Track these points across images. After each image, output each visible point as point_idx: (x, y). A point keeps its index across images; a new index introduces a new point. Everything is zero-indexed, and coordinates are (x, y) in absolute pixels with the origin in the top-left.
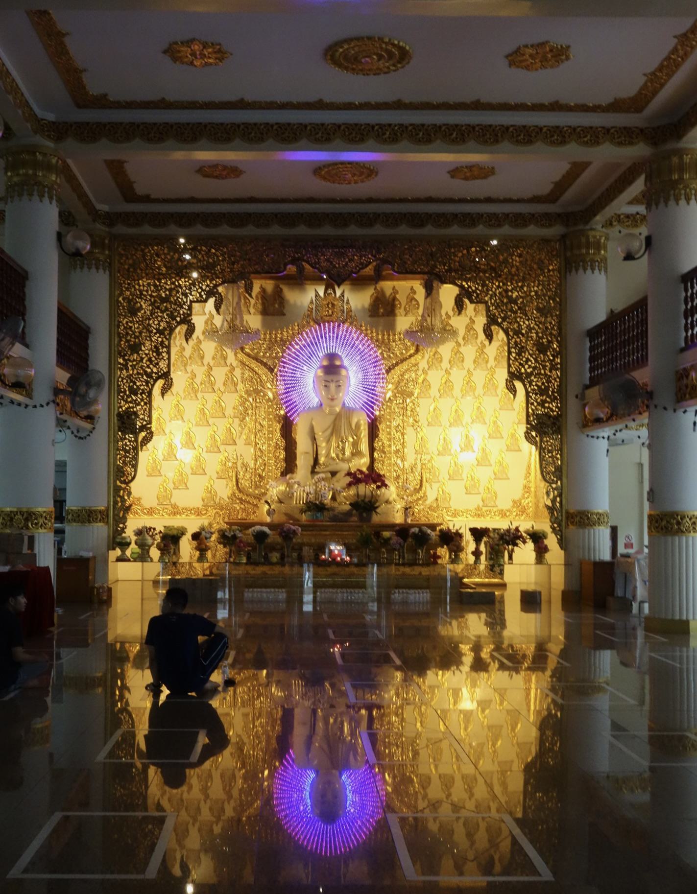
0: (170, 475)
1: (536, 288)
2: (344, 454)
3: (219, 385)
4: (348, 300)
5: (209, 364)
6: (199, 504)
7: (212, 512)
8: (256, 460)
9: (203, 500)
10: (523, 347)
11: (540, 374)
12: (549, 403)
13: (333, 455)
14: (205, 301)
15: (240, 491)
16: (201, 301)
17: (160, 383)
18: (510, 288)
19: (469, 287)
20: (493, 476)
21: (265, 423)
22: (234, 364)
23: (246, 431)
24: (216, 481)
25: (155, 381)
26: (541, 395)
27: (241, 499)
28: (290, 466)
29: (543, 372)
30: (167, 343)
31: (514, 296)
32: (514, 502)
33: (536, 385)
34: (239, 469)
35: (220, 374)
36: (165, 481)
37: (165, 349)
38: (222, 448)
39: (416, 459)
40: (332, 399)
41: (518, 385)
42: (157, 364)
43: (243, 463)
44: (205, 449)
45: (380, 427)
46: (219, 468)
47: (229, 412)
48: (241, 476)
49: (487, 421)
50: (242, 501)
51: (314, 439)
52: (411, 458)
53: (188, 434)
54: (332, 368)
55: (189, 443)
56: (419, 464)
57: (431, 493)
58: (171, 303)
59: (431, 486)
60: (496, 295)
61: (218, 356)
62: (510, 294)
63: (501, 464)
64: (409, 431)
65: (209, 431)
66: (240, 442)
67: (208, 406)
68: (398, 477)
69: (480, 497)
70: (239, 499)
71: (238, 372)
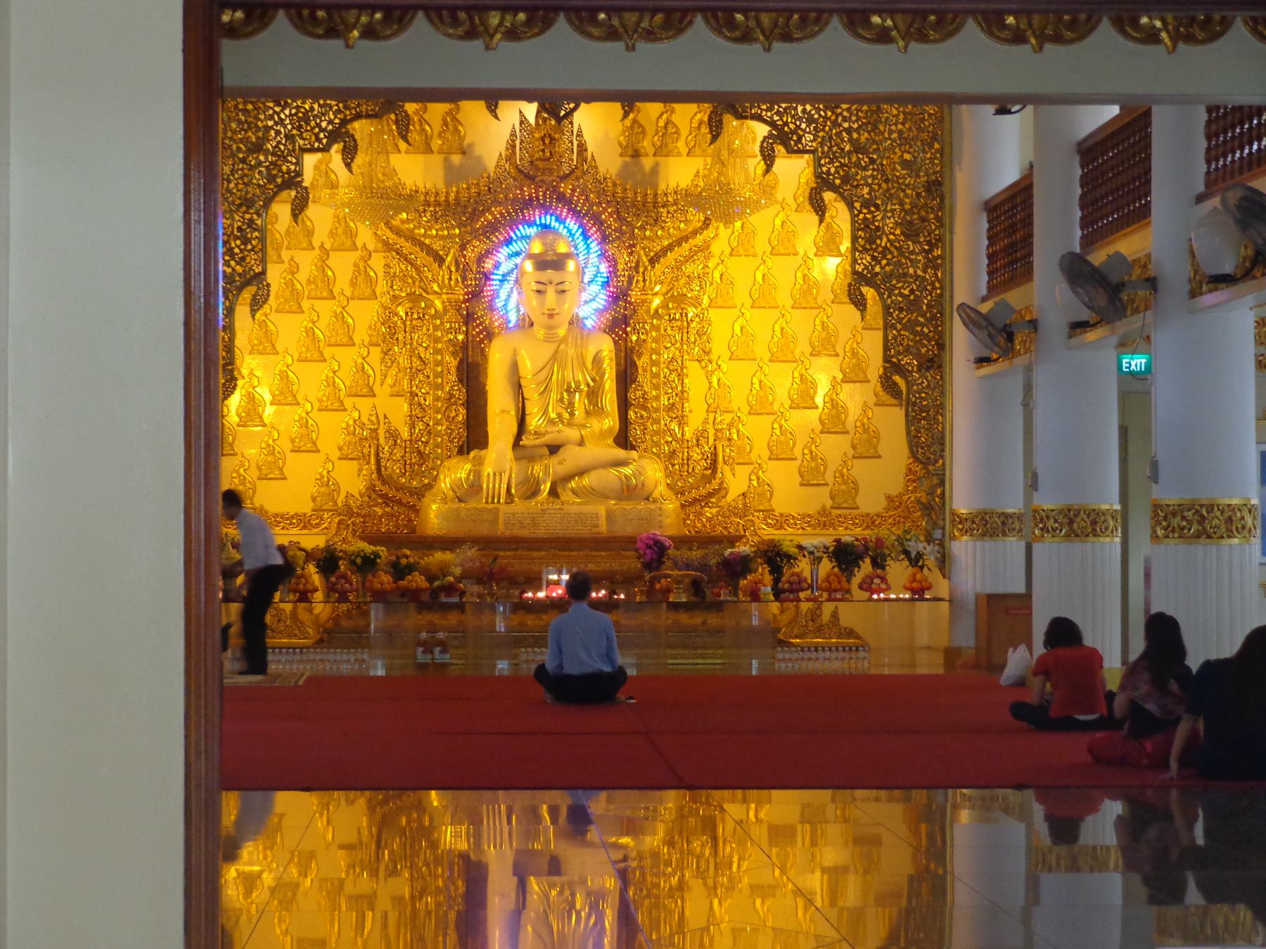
0: (252, 452)
1: (900, 126)
2: (572, 414)
3: (342, 284)
4: (580, 131)
5: (322, 246)
6: (307, 508)
7: (331, 521)
8: (413, 426)
9: (314, 500)
10: (878, 228)
11: (905, 275)
12: (922, 325)
13: (553, 415)
14: (326, 149)
15: (384, 482)
16: (319, 150)
17: (247, 294)
18: (855, 126)
19: (786, 124)
20: (851, 453)
21: (427, 355)
22: (371, 247)
23: (393, 371)
24: (338, 463)
25: (240, 290)
26: (909, 311)
27: (384, 496)
28: (474, 437)
29: (911, 271)
30: (259, 222)
31: (863, 139)
32: (889, 498)
33: (901, 295)
34: (382, 441)
35: (343, 265)
36: (242, 465)
37: (256, 234)
38: (348, 402)
39: (705, 422)
40: (551, 316)
41: (869, 292)
42: (243, 259)
43: (388, 431)
44: (316, 405)
45: (639, 363)
46: (341, 439)
47: (361, 335)
48: (385, 454)
49: (840, 351)
50: (387, 500)
51: (518, 388)
52: (695, 421)
53: (284, 376)
54: (550, 263)
55: (287, 396)
56: (711, 432)
57: (736, 482)
58: (266, 152)
59: (732, 469)
60: (831, 138)
61: (340, 231)
62: (855, 135)
63: (866, 431)
64: (693, 369)
65: (323, 371)
66: (382, 391)
67: (323, 324)
68: (673, 453)
69: (827, 489)
70: (381, 496)
71: (378, 262)
